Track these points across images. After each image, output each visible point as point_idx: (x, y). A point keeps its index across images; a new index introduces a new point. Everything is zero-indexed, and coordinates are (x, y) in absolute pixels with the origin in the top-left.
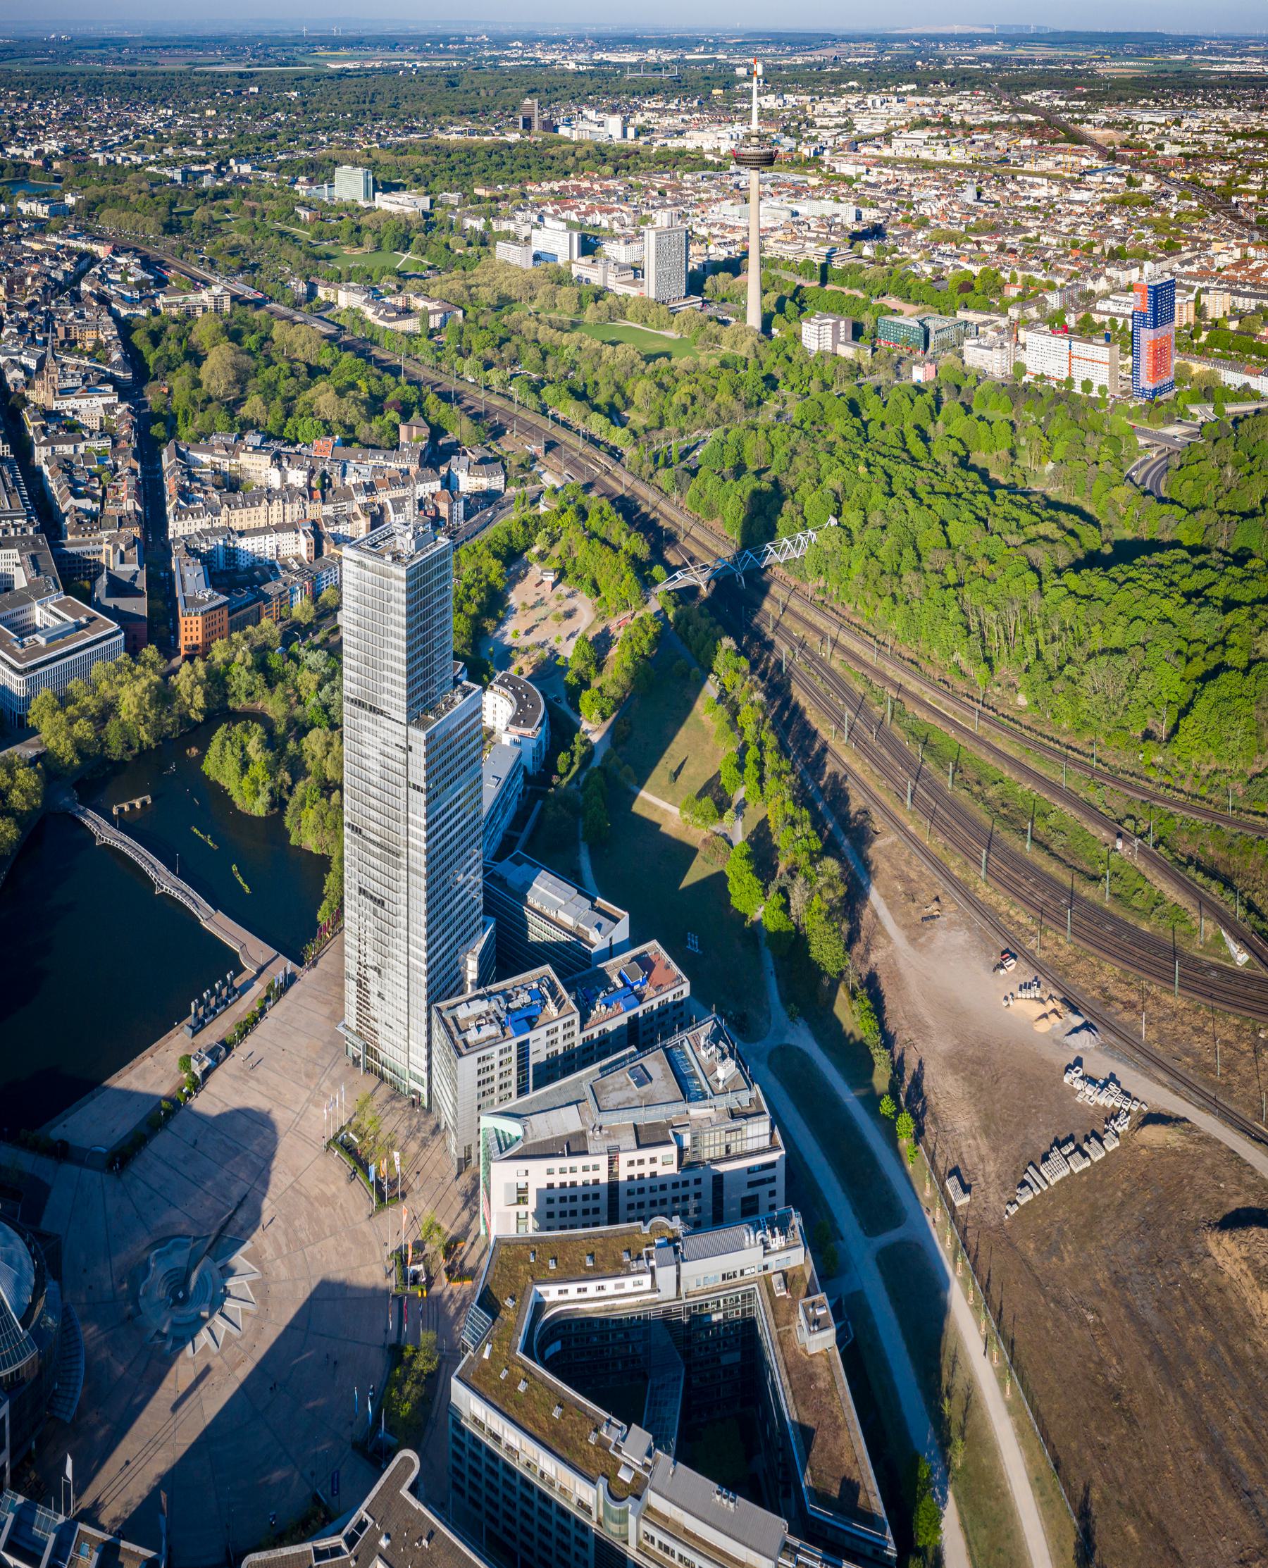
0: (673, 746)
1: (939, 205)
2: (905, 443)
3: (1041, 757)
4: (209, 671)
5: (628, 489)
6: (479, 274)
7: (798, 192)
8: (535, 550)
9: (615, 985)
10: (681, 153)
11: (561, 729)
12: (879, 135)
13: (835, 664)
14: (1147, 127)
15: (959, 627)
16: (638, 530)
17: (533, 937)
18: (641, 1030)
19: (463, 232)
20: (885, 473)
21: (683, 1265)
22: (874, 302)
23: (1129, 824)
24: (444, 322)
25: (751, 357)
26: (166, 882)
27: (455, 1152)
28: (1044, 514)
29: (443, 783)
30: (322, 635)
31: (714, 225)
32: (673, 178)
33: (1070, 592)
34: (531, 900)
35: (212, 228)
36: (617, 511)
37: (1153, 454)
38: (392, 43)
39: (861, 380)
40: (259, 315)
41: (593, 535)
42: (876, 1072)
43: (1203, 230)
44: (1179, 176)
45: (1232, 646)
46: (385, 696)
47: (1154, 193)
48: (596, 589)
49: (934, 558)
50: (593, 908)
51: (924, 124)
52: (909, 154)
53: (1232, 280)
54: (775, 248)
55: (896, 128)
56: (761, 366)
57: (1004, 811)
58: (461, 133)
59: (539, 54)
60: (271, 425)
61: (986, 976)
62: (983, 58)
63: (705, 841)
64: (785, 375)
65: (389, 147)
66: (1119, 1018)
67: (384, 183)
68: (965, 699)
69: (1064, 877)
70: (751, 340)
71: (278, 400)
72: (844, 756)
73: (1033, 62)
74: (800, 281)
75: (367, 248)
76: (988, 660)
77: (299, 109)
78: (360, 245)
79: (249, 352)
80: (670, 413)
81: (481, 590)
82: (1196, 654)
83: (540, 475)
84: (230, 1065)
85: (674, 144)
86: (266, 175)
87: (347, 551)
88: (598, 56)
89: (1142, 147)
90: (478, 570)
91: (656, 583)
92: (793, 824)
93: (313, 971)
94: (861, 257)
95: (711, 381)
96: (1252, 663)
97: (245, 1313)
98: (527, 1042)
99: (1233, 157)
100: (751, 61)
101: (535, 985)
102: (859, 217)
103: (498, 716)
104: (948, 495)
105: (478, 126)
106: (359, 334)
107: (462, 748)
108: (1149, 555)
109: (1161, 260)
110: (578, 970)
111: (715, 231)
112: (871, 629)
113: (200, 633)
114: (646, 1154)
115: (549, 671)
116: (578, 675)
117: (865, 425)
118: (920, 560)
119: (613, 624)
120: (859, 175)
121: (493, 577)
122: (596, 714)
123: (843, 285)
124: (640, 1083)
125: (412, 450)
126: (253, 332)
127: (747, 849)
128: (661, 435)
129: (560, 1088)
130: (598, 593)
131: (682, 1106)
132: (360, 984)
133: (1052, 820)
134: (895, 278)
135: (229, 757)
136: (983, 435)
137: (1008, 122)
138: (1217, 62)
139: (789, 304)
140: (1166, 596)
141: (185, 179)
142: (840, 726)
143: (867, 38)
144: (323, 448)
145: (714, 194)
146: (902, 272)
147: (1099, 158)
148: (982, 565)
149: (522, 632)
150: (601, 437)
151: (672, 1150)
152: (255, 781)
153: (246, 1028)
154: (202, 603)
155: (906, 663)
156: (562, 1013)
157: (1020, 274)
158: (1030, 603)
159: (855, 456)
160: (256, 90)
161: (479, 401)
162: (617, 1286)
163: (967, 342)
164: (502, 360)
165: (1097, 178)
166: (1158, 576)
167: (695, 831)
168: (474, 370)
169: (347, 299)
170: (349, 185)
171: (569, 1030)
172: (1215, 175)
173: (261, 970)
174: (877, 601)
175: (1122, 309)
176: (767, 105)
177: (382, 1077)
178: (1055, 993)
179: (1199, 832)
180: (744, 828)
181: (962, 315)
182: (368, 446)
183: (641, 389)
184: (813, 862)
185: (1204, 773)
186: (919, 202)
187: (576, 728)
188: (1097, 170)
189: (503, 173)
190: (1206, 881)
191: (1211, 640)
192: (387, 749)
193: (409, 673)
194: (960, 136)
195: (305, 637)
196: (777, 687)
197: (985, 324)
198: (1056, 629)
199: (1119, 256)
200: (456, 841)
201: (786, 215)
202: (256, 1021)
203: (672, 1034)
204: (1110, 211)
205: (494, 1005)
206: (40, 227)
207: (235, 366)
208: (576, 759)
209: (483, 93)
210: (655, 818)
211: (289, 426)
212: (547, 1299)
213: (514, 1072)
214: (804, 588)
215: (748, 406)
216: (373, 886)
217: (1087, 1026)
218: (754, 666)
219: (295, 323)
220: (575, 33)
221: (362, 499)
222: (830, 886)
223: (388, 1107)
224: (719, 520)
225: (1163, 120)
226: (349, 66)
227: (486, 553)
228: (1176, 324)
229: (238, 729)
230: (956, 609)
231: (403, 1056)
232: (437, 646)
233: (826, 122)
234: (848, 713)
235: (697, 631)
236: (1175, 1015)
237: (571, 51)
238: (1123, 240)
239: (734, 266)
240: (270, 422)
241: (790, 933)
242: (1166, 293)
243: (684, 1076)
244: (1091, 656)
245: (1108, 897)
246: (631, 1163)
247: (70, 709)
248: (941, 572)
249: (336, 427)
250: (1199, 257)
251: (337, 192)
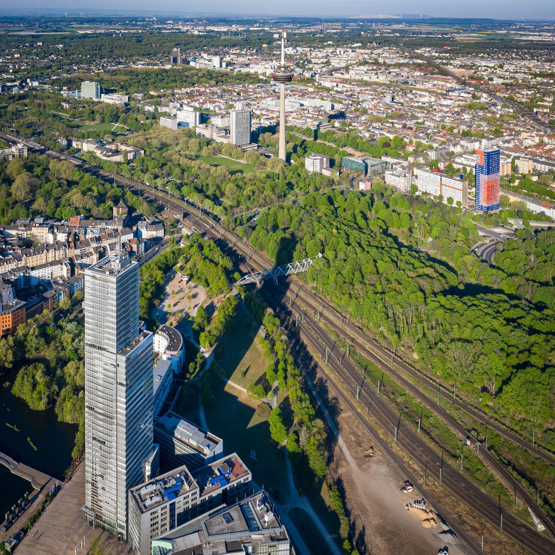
0: (244, 359)
1: (373, 103)
2: (356, 220)
3: (426, 387)
4: (15, 341)
5: (222, 235)
6: (152, 133)
7: (303, 94)
8: (178, 265)
9: (216, 474)
10: (248, 75)
11: (191, 351)
12: (343, 68)
13: (321, 325)
14: (483, 69)
15: (383, 314)
16: (227, 255)
17: (177, 452)
18: (229, 495)
19: (144, 113)
20: (346, 233)
22: (340, 149)
23: (473, 433)
24: (135, 156)
25: (281, 173)
28: (427, 263)
29: (134, 380)
30: (74, 314)
31: (263, 109)
32: (244, 86)
33: (441, 306)
34: (176, 434)
35: (17, 114)
36: (217, 246)
37: (487, 241)
38: (109, 21)
39: (334, 187)
40: (42, 157)
41: (206, 258)
42: (341, 528)
43: (516, 125)
44: (502, 95)
45: (535, 354)
46: (106, 341)
47: (488, 103)
48: (207, 284)
49: (370, 278)
50: (206, 437)
51: (365, 63)
52: (357, 77)
53: (534, 154)
54: (293, 121)
55: (351, 65)
56: (285, 178)
57: (406, 410)
58: (143, 65)
59: (180, 27)
60: (49, 212)
61: (397, 491)
62: (395, 31)
63: (259, 406)
64: (297, 183)
65: (108, 72)
66: (468, 533)
67: (105, 89)
68: (386, 350)
69: (439, 452)
70: (281, 165)
71: (52, 199)
72: (325, 370)
73: (421, 33)
74: (304, 138)
75: (97, 122)
76: (398, 333)
77: (63, 54)
78: (94, 120)
79: (37, 176)
80: (242, 199)
81: (153, 286)
82: (512, 353)
83: (181, 229)
84: (26, 540)
85: (244, 70)
86: (46, 87)
87: (87, 272)
88: (208, 28)
89: (481, 79)
90: (151, 276)
92: (301, 400)
93: (70, 482)
94: (334, 127)
95: (262, 185)
96: (546, 367)
99: (534, 87)
100: (281, 31)
101: (178, 476)
102: (333, 108)
103: (161, 346)
104: (377, 247)
105: (152, 61)
106: (93, 164)
107: (143, 363)
108: (485, 294)
109: (492, 139)
110: (199, 467)
111: (264, 112)
112: (339, 309)
113: (10, 323)
115: (185, 323)
116: (199, 325)
117: (336, 209)
118: (363, 278)
119: (215, 300)
120: (333, 87)
121: (158, 279)
122: (207, 344)
123: (325, 140)
124: (228, 522)
125: (119, 219)
126: (39, 166)
127: (279, 411)
128: (238, 210)
129: (190, 525)
130: (208, 286)
131: (248, 533)
132: (93, 485)
133: (431, 420)
134: (350, 138)
135: (26, 383)
136: (395, 219)
137: (408, 63)
138: (524, 35)
139: (299, 149)
140: (495, 318)
142: (323, 355)
143: (337, 20)
144: (75, 221)
145: (263, 95)
146: (354, 135)
147: (457, 83)
148: (394, 285)
149: (172, 305)
150: (210, 210)
152: (40, 393)
153: (34, 520)
154: (12, 306)
155: (356, 328)
156: (191, 488)
157: (414, 140)
158: (420, 307)
159: (331, 224)
160: (41, 44)
161: (152, 194)
163: (387, 172)
164: (163, 174)
165: (456, 94)
166: (490, 306)
167: (254, 401)
168: (149, 179)
169: (87, 147)
170: (88, 90)
171: (194, 496)
172: (524, 95)
173: (42, 489)
174: (342, 296)
175: (469, 163)
176: (288, 53)
177: (104, 528)
178: (433, 509)
179: (514, 449)
180: (277, 400)
181: (384, 159)
182: (97, 219)
183: (228, 188)
184: (311, 420)
185: (518, 419)
186: (363, 102)
187: (198, 350)
188: (456, 89)
189: (163, 84)
190: (519, 477)
191: (521, 348)
192: (106, 367)
193: (118, 329)
194: (383, 69)
195: (65, 316)
196: (293, 334)
197: (396, 164)
198: (434, 323)
199: (468, 135)
200: (140, 409)
201: (297, 105)
202: (40, 514)
203: (243, 498)
204: (463, 111)
205: (158, 486)
207: (29, 184)
208: (198, 366)
209: (154, 45)
210: (235, 394)
213: (168, 518)
214: (306, 286)
215: (279, 197)
217: (449, 531)
218: (282, 322)
219: (61, 160)
220: (197, 17)
221: (94, 245)
222: (319, 433)
223: (107, 543)
224: (265, 251)
225: (493, 65)
226: (88, 32)
227: (155, 267)
228: (501, 174)
229: (31, 368)
230: (381, 304)
231: (114, 516)
232: (131, 314)
233: (317, 61)
234: (328, 349)
235: (255, 304)
236: (501, 543)
237: (196, 25)
238: (470, 127)
239: (273, 129)
240: (48, 210)
241: (299, 453)
242: (495, 157)
243: (249, 519)
244: (452, 340)
245: (462, 468)
248: (373, 285)
249: (82, 210)
250: (514, 139)
251: (82, 95)
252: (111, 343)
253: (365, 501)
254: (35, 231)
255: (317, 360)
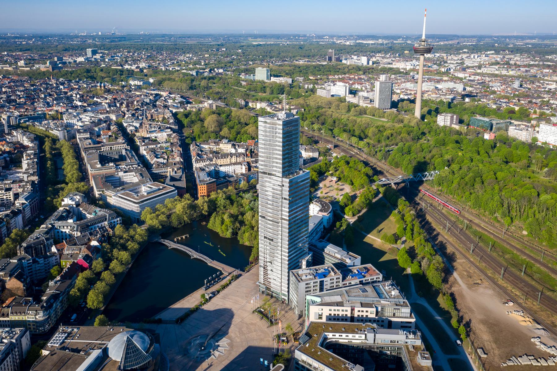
5: (365, 159)
10: (391, 69)
13: (443, 211)
21: (376, 335)
26: (195, 255)
27: (297, 312)
38: (278, 37)
59: (335, 40)
78: (265, 92)
91: (375, 182)
97: (225, 350)
98: (323, 281)
102: (464, 89)
113: (206, 191)
114: (365, 309)
119: (358, 192)
122: (350, 213)
132: (264, 268)
139: (433, 111)
141: (197, 74)
151: (374, 309)
153: (224, 287)
154: (207, 181)
157: (538, 111)
162: (353, 336)
177: (272, 296)
189: (320, 72)
192: (274, 187)
200: (299, 221)
206: (139, 88)
209: (313, 51)
211: (238, 137)
212: (328, 337)
216: (269, 235)
226: (261, 43)
233: (452, 62)
246: (359, 311)
247: (157, 213)
252: (278, 170)
253: (472, 305)
254: (221, 146)
255: (439, 230)
